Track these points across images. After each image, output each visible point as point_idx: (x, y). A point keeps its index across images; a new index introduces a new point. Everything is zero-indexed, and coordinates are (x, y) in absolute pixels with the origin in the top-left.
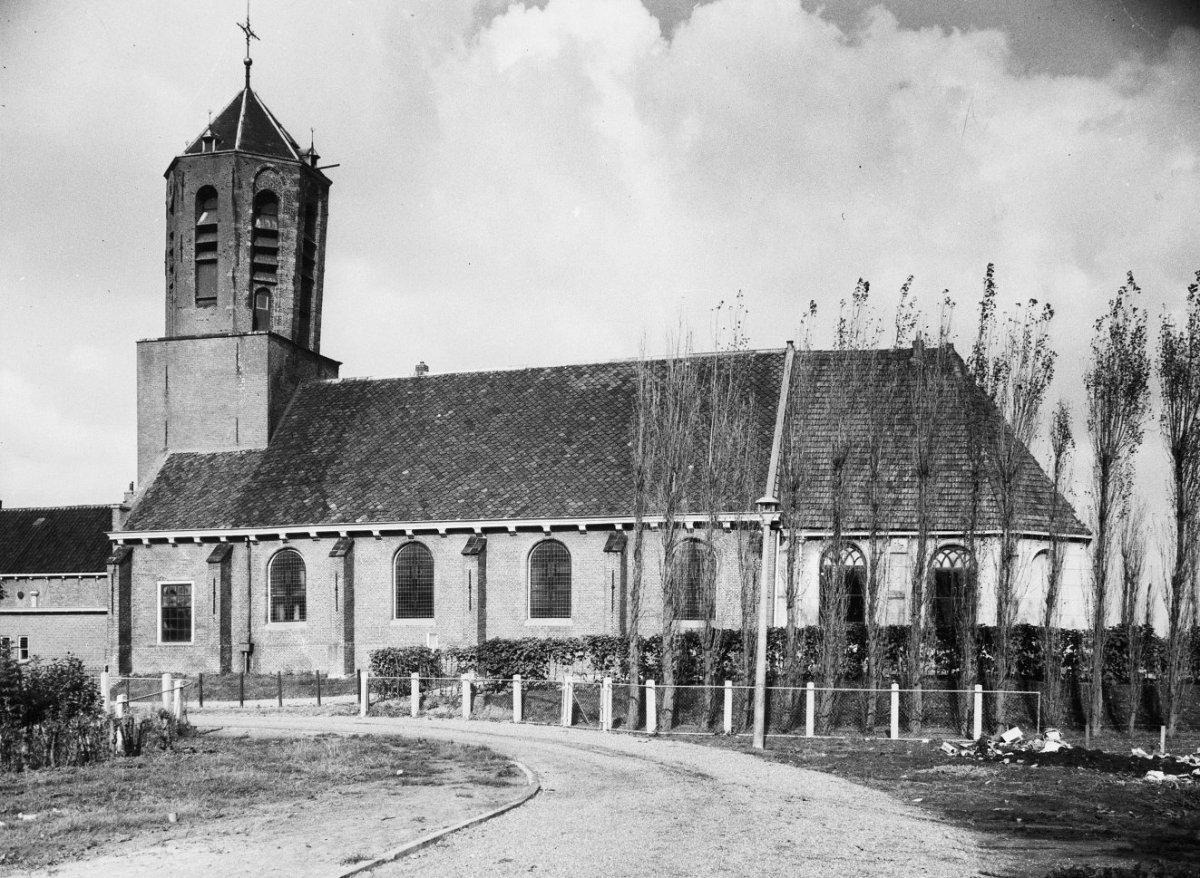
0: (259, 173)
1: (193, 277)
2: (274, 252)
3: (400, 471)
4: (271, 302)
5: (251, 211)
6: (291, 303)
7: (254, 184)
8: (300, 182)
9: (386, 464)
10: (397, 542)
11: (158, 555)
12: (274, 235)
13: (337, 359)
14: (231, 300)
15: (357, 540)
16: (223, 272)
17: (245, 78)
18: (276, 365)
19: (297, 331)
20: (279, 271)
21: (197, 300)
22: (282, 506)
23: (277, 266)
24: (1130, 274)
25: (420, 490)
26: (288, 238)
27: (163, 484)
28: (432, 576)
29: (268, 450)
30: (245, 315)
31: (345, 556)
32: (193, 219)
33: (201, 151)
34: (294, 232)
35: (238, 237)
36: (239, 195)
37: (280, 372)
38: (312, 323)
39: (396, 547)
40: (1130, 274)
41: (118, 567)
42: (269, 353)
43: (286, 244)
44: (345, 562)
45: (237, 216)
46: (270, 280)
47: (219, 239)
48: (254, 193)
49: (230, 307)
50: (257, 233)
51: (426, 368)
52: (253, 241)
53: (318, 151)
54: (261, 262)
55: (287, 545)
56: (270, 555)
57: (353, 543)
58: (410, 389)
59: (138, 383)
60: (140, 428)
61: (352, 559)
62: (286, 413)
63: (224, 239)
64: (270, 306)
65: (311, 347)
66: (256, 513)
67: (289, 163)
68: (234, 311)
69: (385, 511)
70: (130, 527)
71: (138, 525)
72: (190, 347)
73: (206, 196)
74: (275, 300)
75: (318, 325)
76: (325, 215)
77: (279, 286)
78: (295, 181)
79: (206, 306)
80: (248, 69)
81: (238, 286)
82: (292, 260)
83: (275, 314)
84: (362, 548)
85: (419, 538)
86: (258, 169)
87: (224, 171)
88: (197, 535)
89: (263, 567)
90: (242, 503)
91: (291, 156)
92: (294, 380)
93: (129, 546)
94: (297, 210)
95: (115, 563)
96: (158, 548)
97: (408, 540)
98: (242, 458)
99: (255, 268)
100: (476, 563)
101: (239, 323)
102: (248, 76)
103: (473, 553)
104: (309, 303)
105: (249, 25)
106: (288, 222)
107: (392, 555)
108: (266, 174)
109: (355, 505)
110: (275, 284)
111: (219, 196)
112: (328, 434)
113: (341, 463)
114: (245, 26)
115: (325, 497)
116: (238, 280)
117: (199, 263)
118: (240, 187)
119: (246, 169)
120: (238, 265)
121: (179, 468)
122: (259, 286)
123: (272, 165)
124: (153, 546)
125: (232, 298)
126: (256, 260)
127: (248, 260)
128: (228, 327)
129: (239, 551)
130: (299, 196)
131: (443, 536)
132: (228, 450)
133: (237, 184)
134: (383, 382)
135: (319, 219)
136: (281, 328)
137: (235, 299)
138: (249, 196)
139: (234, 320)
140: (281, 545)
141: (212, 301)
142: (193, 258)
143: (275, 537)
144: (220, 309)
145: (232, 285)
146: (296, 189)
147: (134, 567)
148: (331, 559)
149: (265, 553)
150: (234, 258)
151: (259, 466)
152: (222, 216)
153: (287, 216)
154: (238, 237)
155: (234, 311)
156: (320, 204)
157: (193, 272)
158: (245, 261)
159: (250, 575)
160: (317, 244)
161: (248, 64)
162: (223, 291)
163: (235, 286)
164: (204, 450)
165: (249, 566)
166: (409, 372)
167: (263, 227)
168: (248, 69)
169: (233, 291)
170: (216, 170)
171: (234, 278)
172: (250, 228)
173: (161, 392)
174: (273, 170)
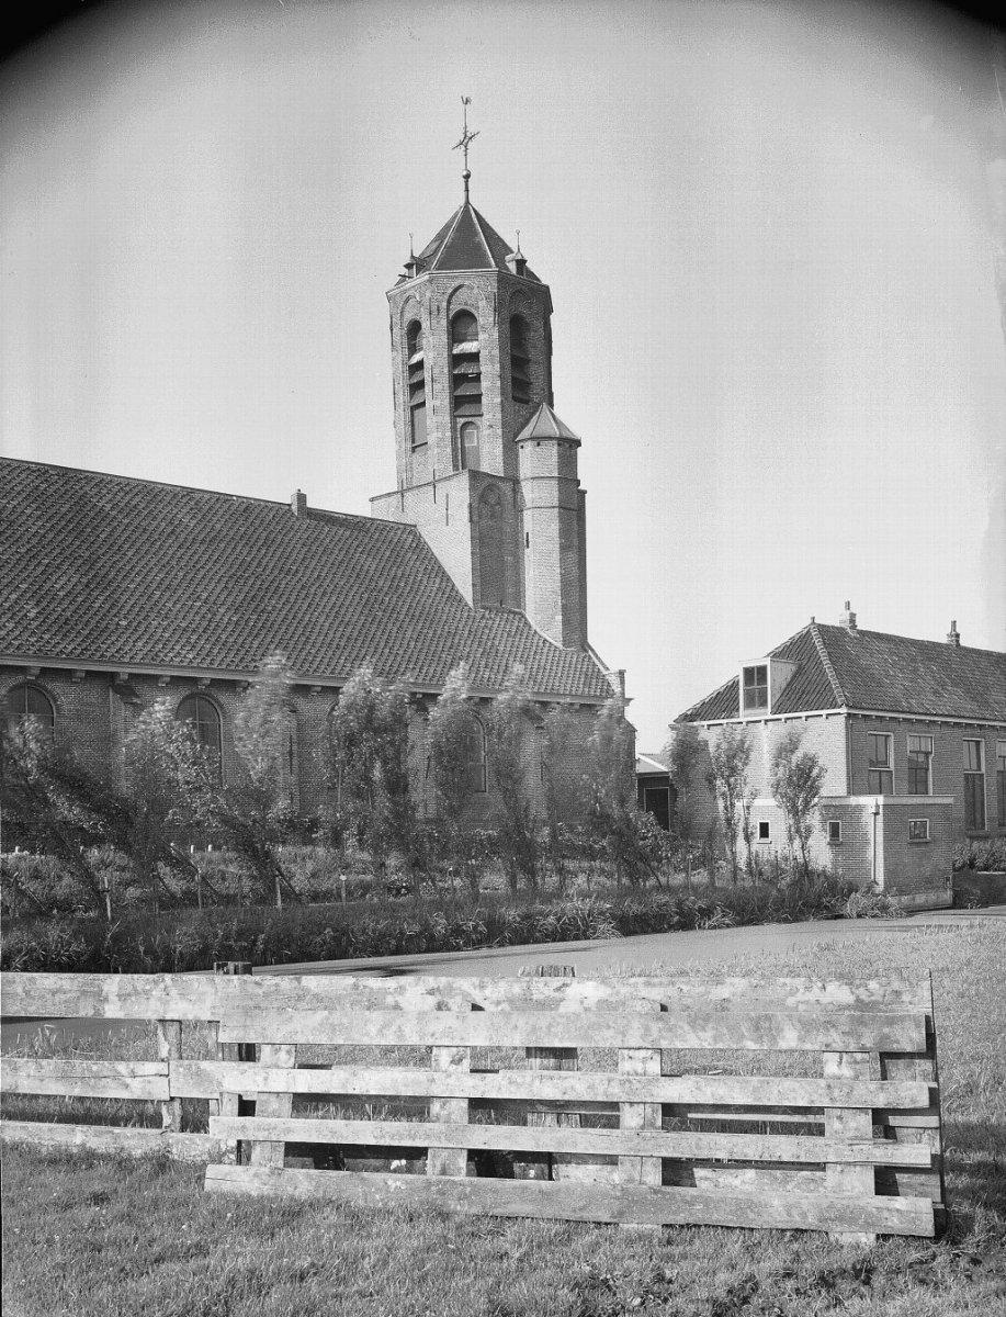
50: (457, 360)
114: (469, 135)
126: (459, 392)
161: (467, 177)
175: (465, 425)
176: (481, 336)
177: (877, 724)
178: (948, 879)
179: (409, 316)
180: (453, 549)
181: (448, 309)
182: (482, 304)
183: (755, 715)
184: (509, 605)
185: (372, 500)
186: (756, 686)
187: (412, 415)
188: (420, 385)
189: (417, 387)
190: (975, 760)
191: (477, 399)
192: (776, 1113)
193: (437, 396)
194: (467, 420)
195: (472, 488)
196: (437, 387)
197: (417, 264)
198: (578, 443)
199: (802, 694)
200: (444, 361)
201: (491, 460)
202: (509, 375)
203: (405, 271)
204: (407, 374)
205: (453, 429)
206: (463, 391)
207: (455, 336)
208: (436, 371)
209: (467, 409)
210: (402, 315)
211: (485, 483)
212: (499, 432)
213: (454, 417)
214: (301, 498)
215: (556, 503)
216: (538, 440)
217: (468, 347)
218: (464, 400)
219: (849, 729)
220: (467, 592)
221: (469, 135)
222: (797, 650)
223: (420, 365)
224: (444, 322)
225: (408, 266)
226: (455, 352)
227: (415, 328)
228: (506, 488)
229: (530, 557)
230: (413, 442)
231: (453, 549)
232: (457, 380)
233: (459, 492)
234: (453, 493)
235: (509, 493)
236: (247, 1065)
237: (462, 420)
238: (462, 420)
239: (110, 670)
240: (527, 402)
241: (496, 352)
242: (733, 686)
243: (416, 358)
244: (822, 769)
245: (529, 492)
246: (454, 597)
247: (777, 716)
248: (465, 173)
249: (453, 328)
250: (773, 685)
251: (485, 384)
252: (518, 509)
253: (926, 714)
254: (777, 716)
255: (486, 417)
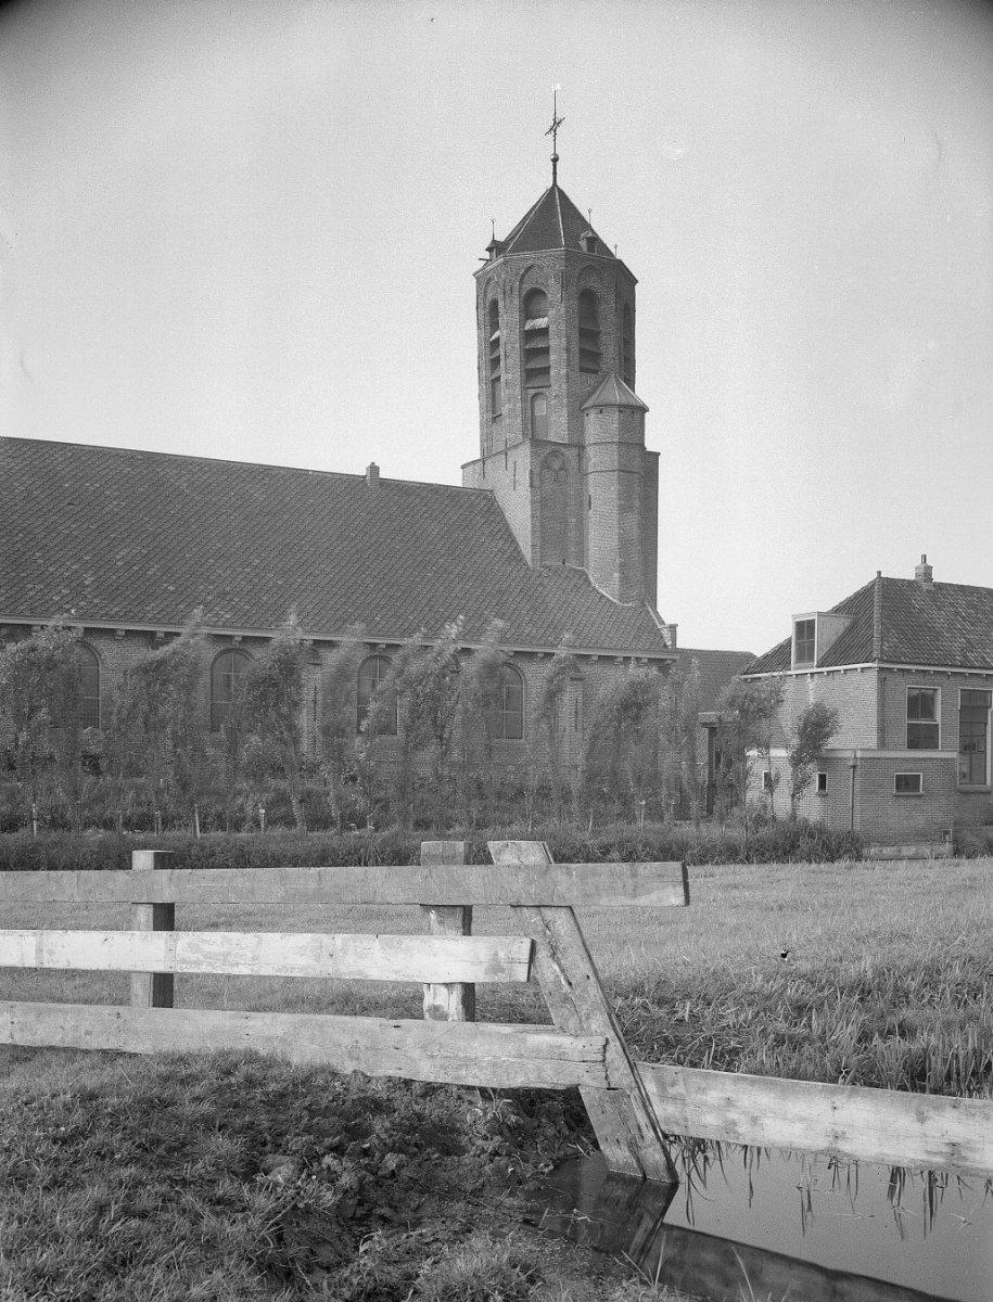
126: (531, 365)
161: (555, 160)
176: (551, 312)
177: (920, 678)
178: (946, 833)
179: (490, 296)
180: (519, 510)
181: (520, 289)
182: (552, 281)
183: (804, 668)
184: (572, 564)
185: (463, 467)
186: (805, 640)
187: (493, 388)
189: (495, 362)
191: (546, 371)
193: (511, 372)
195: (534, 454)
196: (510, 361)
197: (496, 247)
198: (643, 409)
199: (844, 651)
200: (516, 335)
201: (558, 430)
202: (575, 349)
203: (487, 255)
205: (523, 400)
206: (536, 364)
207: (528, 313)
208: (509, 347)
209: (537, 382)
210: (485, 296)
211: (548, 449)
212: (565, 401)
213: (525, 389)
214: (374, 469)
215: (616, 466)
216: (601, 408)
217: (541, 323)
218: (535, 373)
219: (882, 682)
220: (527, 551)
222: (855, 606)
223: (496, 343)
224: (516, 302)
225: (489, 249)
226: (526, 328)
228: (571, 453)
229: (592, 516)
230: (494, 412)
231: (519, 510)
232: (529, 354)
233: (523, 458)
234: (519, 461)
235: (574, 462)
236: (161, 968)
237: (532, 392)
238: (532, 392)
239: (111, 627)
240: (595, 372)
241: (563, 327)
242: (790, 639)
245: (594, 457)
246: (517, 556)
247: (820, 670)
249: (526, 306)
250: (822, 640)
251: (553, 357)
252: (583, 474)
253: (983, 668)
254: (820, 670)
255: (555, 387)
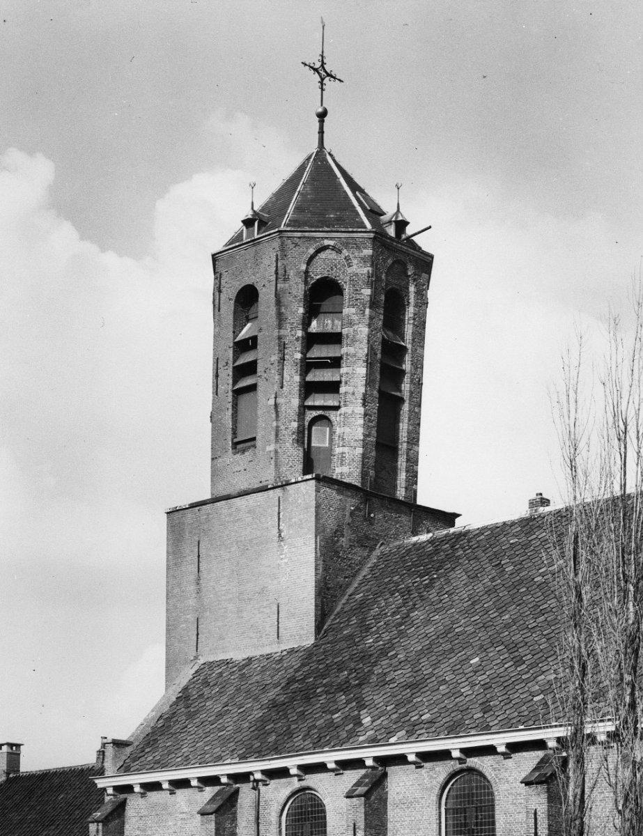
0: (312, 258)
1: (230, 412)
2: (336, 363)
3: (468, 659)
4: (332, 433)
5: (301, 310)
6: (359, 433)
7: (306, 272)
8: (374, 261)
9: (452, 650)
10: (442, 770)
11: (154, 806)
12: (335, 338)
13: (448, 509)
14: (273, 437)
15: (392, 770)
16: (264, 399)
17: (317, 136)
18: (331, 524)
19: (372, 473)
20: (343, 389)
21: (235, 445)
22: (304, 726)
23: (340, 382)
24: (303, 63)
25: (486, 686)
26: (354, 341)
27: (182, 704)
28: (493, 823)
29: (315, 645)
30: (293, 455)
31: (366, 795)
32: (231, 335)
33: (242, 240)
34: (364, 331)
35: (283, 347)
36: (284, 291)
37: (338, 532)
38: (402, 462)
39: (442, 778)
40: (303, 63)
41: (100, 825)
42: (318, 506)
43: (351, 350)
44: (367, 805)
45: (281, 319)
46: (330, 403)
47: (260, 356)
48: (306, 283)
49: (271, 448)
50: (311, 340)
51: (545, 502)
52: (304, 353)
53: (406, 215)
54: (317, 379)
55: (304, 784)
56: (282, 801)
57: (385, 775)
58: (515, 536)
59: (168, 569)
60: (168, 630)
61: (383, 801)
62: (350, 590)
63: (265, 356)
64: (331, 440)
65: (401, 493)
66: (272, 738)
67: (355, 235)
68: (276, 452)
69: (431, 722)
70: (126, 769)
71: (136, 765)
72: (225, 511)
73: (247, 297)
74: (338, 431)
75: (413, 461)
76: (423, 303)
77: (343, 410)
78: (364, 260)
79: (243, 451)
80: (322, 122)
81: (282, 415)
82: (362, 371)
83: (338, 450)
84: (400, 783)
85: (473, 762)
86: (311, 251)
87: (266, 262)
88: (193, 774)
89: (273, 818)
90: (260, 728)
91: (362, 225)
92: (367, 542)
93: (122, 796)
94: (368, 299)
95: (98, 822)
96: (154, 796)
97: (458, 766)
98: (281, 660)
99: (308, 389)
100: (543, 798)
101: (283, 469)
102: (321, 132)
103: (538, 782)
104: (396, 431)
105: (323, 64)
106: (355, 318)
107: (437, 791)
108: (322, 255)
109: (394, 716)
110: (337, 408)
111: (260, 295)
112: (394, 614)
113: (396, 655)
114: (318, 65)
115: (361, 706)
116: (282, 409)
117: (238, 393)
118: (286, 279)
119: (293, 252)
120: (282, 387)
121: (206, 683)
122: (315, 413)
123: (332, 243)
124: (149, 794)
125: (273, 433)
126: (310, 378)
127: (297, 378)
128: (269, 477)
129: (246, 794)
130: (374, 281)
131: (506, 756)
132: (267, 650)
133: (281, 275)
134: (482, 530)
135: (410, 311)
136: (345, 469)
137: (277, 435)
138: (298, 289)
139: (276, 465)
140: (295, 784)
141: (252, 443)
142: (230, 386)
143: (283, 773)
144: (259, 451)
145: (274, 416)
146: (367, 269)
147: (127, 826)
148: (348, 800)
149: (277, 793)
150: (277, 377)
151: (297, 671)
152: (262, 325)
153: (353, 310)
154: (283, 347)
155: (276, 452)
156: (412, 289)
157: (230, 406)
158: (293, 378)
159: (258, 829)
160: (409, 346)
161: (322, 116)
162: (263, 427)
163: (277, 416)
164: (238, 656)
165: (258, 818)
166: (520, 510)
167: (320, 330)
168: (322, 122)
169: (275, 424)
170: (257, 262)
171: (276, 405)
172: (300, 333)
173: (193, 577)
174: (334, 248)
175: (314, 421)
187: (235, 406)
188: (251, 368)
190: (359, 234)
192: (308, 437)
194: (320, 412)
204: (230, 353)
206: (317, 376)
221: (318, 65)
227: (247, 297)
243: (245, 333)
244: (537, 495)
248: (320, 110)
